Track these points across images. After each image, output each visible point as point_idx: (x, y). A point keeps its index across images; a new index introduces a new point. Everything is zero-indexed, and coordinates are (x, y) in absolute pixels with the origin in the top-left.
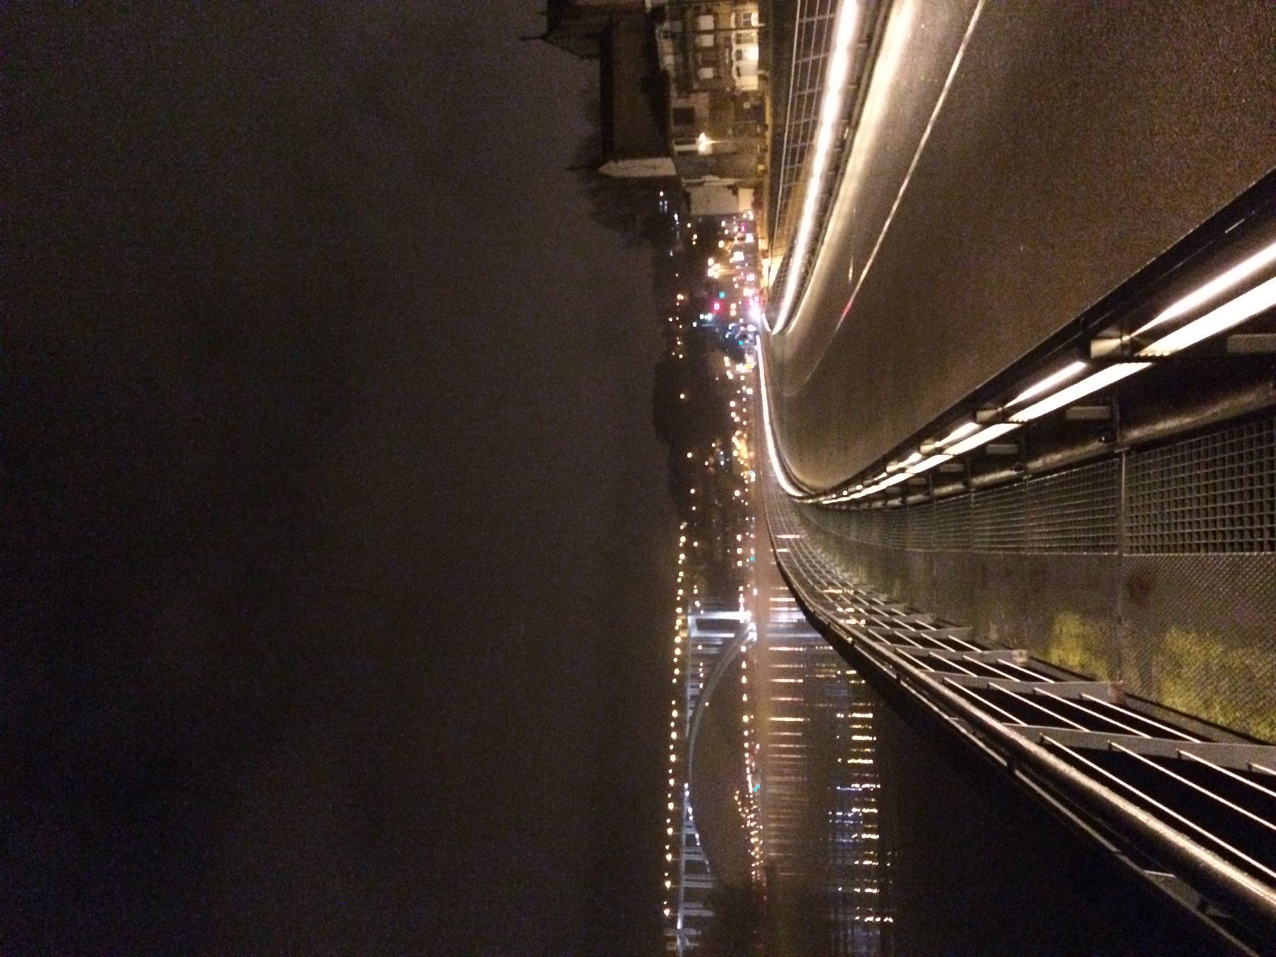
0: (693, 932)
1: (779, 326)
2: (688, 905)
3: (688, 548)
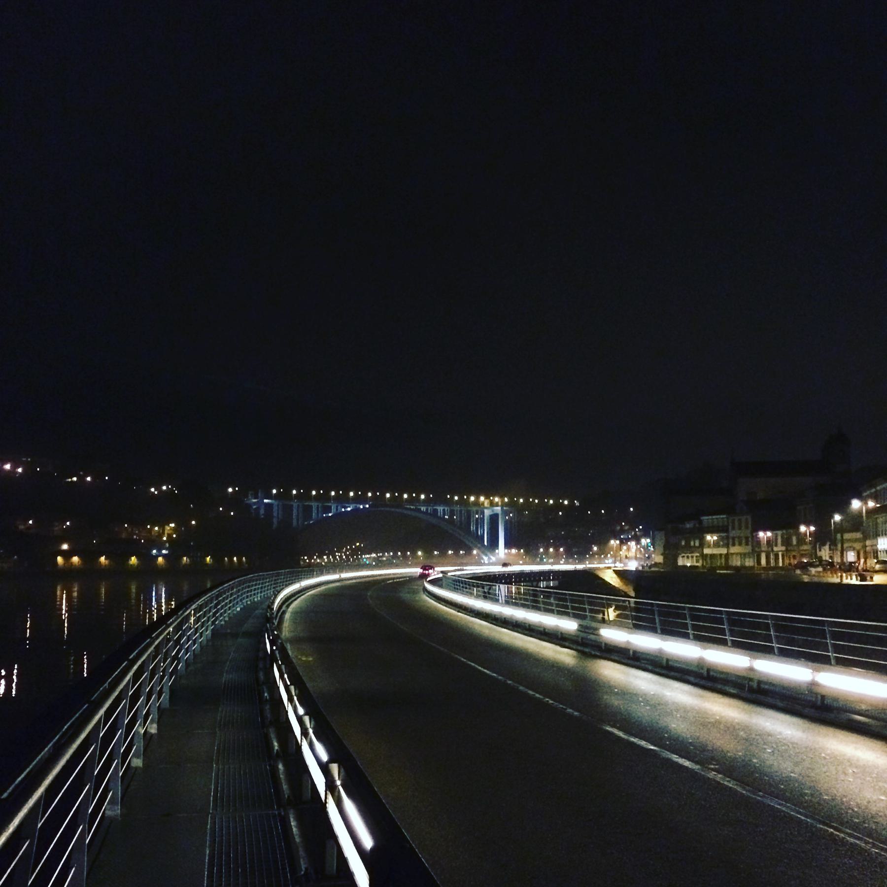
0: (262, 511)
1: (429, 587)
2: (301, 509)
3: (558, 506)
